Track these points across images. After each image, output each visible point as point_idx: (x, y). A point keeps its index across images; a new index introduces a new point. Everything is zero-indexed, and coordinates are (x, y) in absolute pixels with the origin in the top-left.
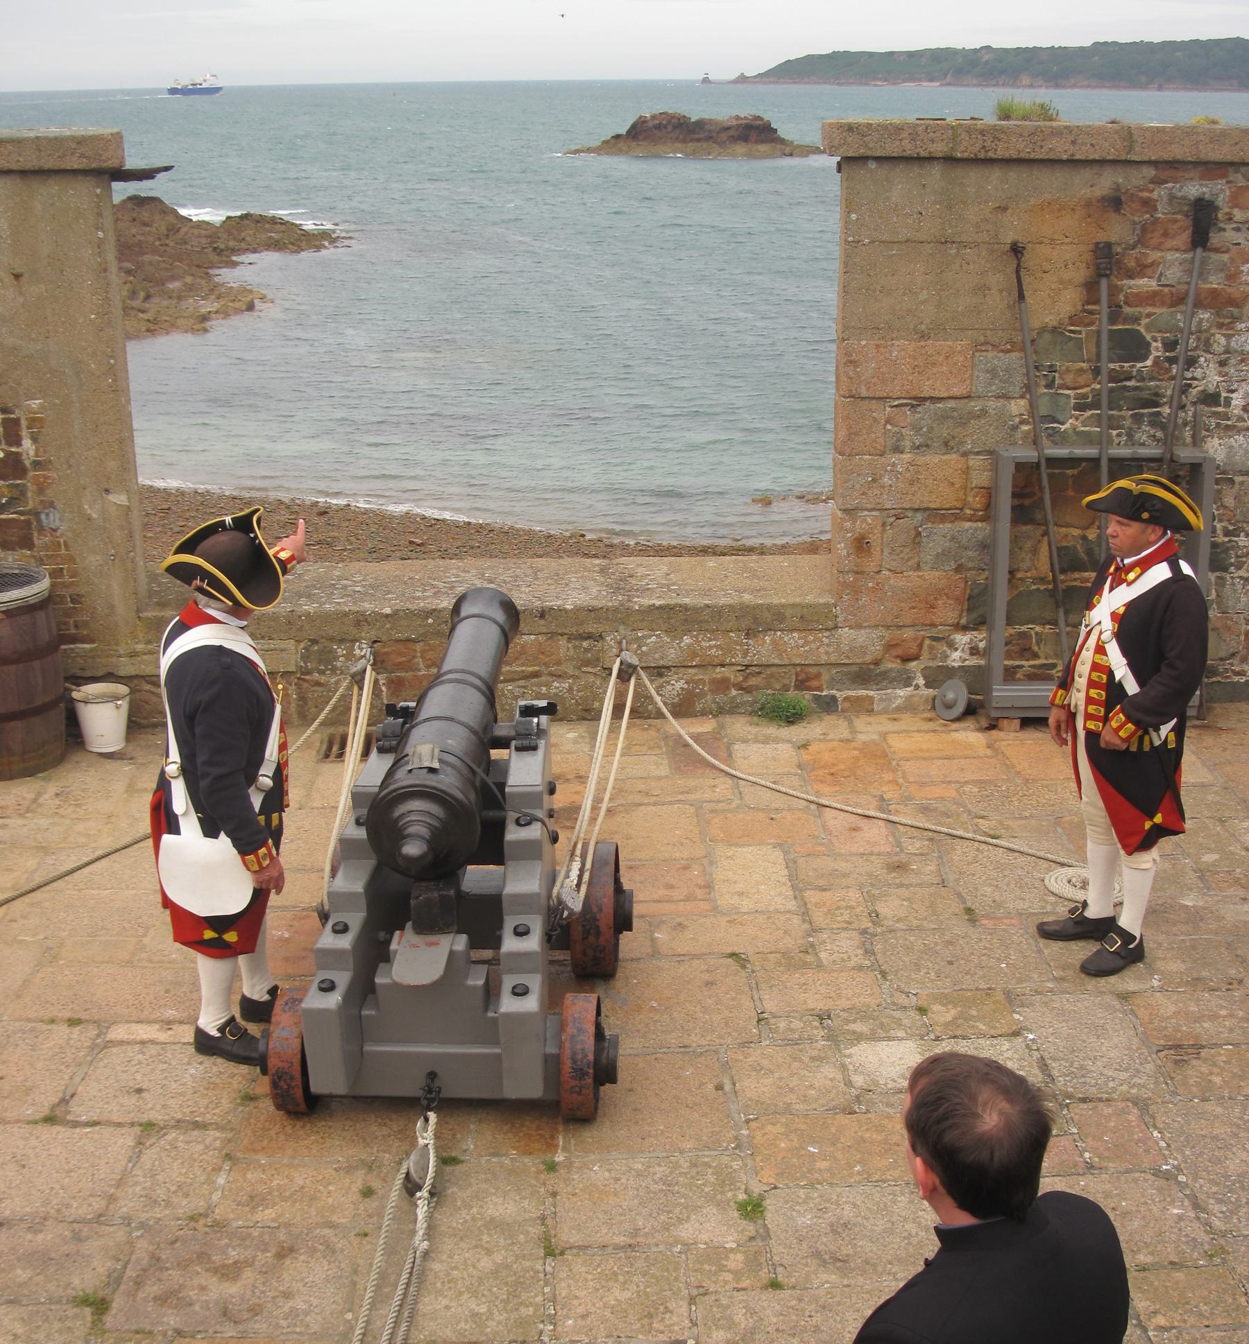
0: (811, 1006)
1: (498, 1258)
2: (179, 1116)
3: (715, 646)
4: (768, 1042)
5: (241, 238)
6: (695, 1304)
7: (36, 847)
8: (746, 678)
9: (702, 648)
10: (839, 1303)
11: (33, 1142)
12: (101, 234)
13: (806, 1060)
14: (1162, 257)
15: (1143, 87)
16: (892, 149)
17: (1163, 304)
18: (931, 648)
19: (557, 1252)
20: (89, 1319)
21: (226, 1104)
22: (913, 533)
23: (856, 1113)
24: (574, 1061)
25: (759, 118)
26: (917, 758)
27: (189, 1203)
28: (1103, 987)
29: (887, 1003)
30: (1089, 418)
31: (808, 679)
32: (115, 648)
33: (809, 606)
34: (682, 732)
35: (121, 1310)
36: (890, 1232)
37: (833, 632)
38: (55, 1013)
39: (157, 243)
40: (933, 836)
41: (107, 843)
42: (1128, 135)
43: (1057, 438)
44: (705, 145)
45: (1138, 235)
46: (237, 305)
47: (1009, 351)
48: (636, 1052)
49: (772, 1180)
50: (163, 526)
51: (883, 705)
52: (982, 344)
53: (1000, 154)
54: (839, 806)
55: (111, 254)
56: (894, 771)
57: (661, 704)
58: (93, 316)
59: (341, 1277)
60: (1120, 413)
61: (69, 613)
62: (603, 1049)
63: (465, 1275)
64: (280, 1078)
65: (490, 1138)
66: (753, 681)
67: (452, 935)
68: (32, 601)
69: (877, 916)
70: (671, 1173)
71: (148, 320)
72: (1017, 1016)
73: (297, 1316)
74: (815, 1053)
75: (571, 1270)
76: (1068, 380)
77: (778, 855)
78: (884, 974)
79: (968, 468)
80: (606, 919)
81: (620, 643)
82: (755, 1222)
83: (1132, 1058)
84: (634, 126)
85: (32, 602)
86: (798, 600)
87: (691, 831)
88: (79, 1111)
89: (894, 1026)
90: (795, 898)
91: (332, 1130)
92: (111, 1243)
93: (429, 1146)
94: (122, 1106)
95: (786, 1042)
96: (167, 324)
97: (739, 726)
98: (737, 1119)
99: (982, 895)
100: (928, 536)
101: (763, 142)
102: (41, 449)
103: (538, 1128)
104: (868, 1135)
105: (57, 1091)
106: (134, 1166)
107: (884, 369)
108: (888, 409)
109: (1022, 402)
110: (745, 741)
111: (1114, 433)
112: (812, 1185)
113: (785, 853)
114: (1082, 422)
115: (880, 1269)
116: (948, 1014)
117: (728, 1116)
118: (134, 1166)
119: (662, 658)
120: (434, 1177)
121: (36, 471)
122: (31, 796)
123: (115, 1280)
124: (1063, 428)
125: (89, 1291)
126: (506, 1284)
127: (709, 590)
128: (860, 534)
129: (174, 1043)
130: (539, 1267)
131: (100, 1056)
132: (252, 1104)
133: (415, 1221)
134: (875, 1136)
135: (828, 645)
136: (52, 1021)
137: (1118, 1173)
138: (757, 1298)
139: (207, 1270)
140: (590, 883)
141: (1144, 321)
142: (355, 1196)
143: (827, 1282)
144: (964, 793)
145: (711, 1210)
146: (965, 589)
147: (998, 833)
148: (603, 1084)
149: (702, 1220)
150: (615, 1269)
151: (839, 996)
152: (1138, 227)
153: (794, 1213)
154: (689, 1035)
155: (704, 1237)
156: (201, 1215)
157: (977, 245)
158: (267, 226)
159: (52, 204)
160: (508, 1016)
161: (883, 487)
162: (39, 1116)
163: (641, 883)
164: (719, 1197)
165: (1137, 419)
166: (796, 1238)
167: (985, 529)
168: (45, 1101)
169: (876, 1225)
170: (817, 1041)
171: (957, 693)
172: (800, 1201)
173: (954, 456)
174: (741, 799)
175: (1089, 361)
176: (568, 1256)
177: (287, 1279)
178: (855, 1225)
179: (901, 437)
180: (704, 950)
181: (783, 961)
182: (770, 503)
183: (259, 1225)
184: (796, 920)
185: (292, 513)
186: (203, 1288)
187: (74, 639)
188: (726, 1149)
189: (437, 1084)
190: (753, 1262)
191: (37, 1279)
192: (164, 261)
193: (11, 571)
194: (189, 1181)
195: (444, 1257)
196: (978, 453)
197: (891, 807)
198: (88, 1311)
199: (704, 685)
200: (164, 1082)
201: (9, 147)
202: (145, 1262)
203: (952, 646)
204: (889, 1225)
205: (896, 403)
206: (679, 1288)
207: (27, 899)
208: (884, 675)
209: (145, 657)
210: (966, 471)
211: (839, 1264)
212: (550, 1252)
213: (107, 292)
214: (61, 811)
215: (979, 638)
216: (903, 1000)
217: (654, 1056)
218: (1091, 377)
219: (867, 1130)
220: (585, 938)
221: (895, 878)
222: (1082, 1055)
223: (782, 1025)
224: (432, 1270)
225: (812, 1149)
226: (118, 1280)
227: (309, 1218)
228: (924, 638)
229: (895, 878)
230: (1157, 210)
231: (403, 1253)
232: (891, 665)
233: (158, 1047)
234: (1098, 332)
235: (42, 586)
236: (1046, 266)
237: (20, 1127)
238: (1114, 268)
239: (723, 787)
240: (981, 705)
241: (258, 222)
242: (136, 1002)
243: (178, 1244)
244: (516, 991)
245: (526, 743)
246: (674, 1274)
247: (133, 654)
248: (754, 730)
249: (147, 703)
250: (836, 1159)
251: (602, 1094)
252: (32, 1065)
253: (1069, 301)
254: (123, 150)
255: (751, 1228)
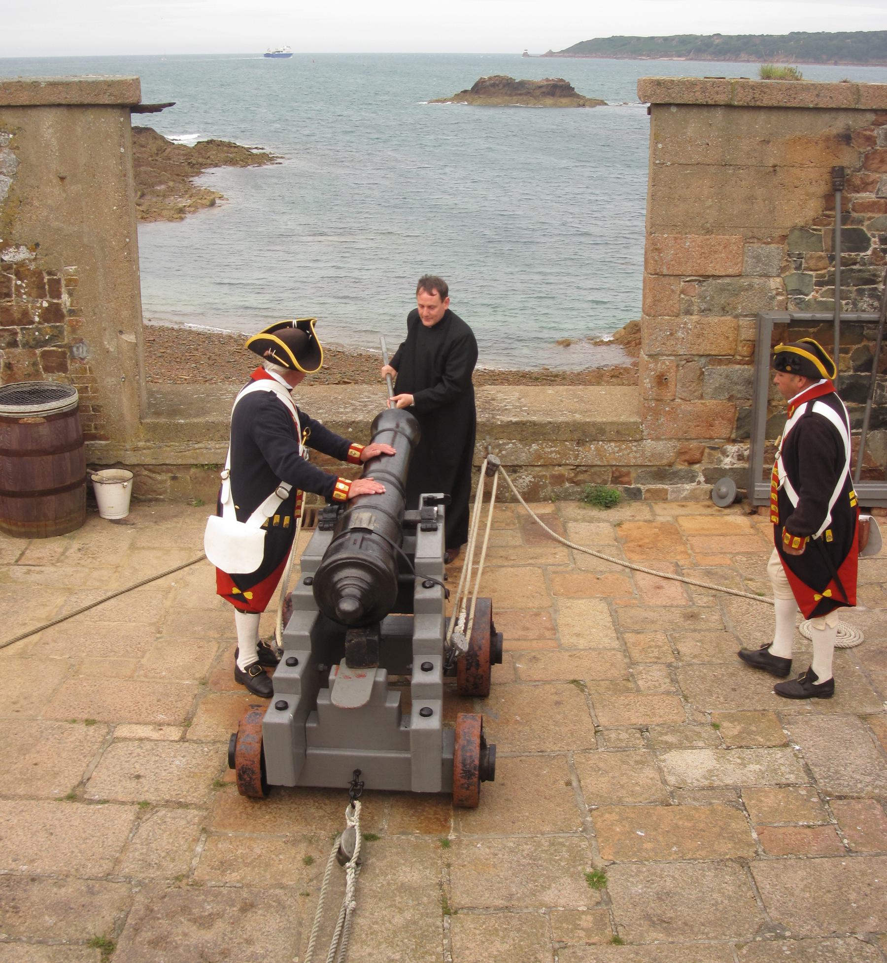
0: (634, 721)
1: (408, 915)
2: (167, 797)
3: (555, 451)
4: (603, 749)
5: (207, 156)
6: (558, 955)
7: (64, 589)
8: (576, 475)
9: (545, 453)
10: (666, 957)
11: (59, 815)
12: (122, 150)
13: (632, 763)
14: (878, 178)
15: (824, 62)
16: (688, 98)
17: (880, 211)
18: (710, 455)
19: (452, 911)
20: (99, 957)
21: (203, 789)
22: (698, 372)
23: (671, 805)
24: (464, 765)
25: (562, 80)
26: (701, 535)
27: (175, 866)
28: (848, 709)
29: (689, 720)
30: (826, 291)
31: (621, 476)
32: (123, 444)
33: (623, 424)
34: (532, 513)
35: (123, 951)
36: (702, 900)
37: (640, 443)
38: (76, 715)
39: (150, 159)
40: (716, 594)
41: (115, 586)
42: (856, 90)
43: (803, 306)
44: (525, 98)
45: (862, 161)
46: (204, 202)
47: (769, 243)
48: (506, 755)
49: (611, 857)
50: (150, 352)
51: (674, 495)
52: (750, 238)
53: (766, 102)
54: (646, 570)
55: (129, 165)
56: (685, 544)
57: (517, 493)
58: (115, 208)
59: (290, 928)
60: (848, 288)
61: (90, 419)
62: (485, 755)
63: (384, 929)
64: (244, 772)
65: (399, 820)
66: (581, 477)
67: (375, 669)
68: (65, 410)
69: (678, 653)
70: (536, 850)
71: (143, 211)
72: (785, 732)
73: (257, 959)
74: (638, 758)
75: (463, 926)
76: (811, 265)
77: (603, 606)
78: (686, 698)
79: (738, 326)
80: (484, 654)
81: (486, 448)
82: (600, 890)
83: (873, 765)
84: (476, 85)
85: (64, 411)
86: (615, 419)
87: (540, 587)
88: (94, 791)
89: (695, 738)
90: (618, 638)
91: (282, 811)
92: (116, 897)
93: (356, 827)
94: (125, 788)
95: (616, 749)
96: (155, 214)
97: (571, 509)
98: (582, 808)
99: (754, 638)
100: (709, 375)
101: (564, 96)
102: (75, 302)
103: (435, 813)
104: (681, 823)
105: (77, 776)
106: (134, 836)
107: (680, 255)
108: (682, 284)
109: (778, 280)
110: (576, 520)
111: (844, 302)
112: (641, 862)
113: (609, 604)
114: (821, 294)
115: (696, 929)
116: (736, 729)
117: (576, 806)
118: (134, 836)
119: (516, 459)
120: (359, 852)
121: (70, 316)
122: (60, 550)
123: (119, 926)
124: (807, 298)
125: (100, 935)
126: (414, 936)
127: (551, 410)
128: (660, 372)
129: (164, 741)
130: (439, 923)
131: (109, 749)
132: (222, 789)
133: (346, 884)
134: (686, 824)
135: (636, 452)
136: (74, 721)
137: (870, 855)
138: (604, 952)
139: (189, 920)
140: (473, 629)
141: (866, 223)
142: (300, 864)
143: (656, 939)
144: (736, 561)
145: (566, 880)
146: (735, 413)
147: (762, 592)
148: (483, 781)
149: (560, 888)
150: (496, 926)
151: (654, 714)
152: (863, 156)
153: (629, 884)
154: (545, 742)
155: (562, 901)
156: (184, 876)
157: (748, 167)
158: (225, 148)
159: (89, 129)
160: (417, 732)
161: (677, 339)
162: (63, 795)
163: (505, 625)
164: (572, 869)
165: (860, 292)
166: (632, 904)
167: (750, 371)
168: (67, 783)
169: (691, 894)
170: (639, 749)
171: (729, 488)
172: (633, 874)
173: (729, 318)
174: (575, 563)
175: (827, 250)
176: (460, 915)
177: (249, 929)
178: (674, 894)
179: (691, 304)
180: (552, 677)
181: (611, 686)
182: (568, 345)
183: (227, 885)
184: (619, 656)
185: (238, 345)
186: (185, 935)
187: (94, 437)
188: (576, 832)
189: (360, 780)
190: (600, 923)
191: (59, 924)
192: (154, 171)
193: (50, 388)
194: (175, 848)
195: (367, 914)
196: (746, 316)
197: (684, 571)
198: (98, 951)
199: (546, 479)
200: (157, 771)
201: (60, 88)
202: (142, 912)
203: (725, 453)
204: (701, 894)
205: (687, 279)
206: (545, 942)
207: (57, 627)
208: (675, 474)
209: (144, 451)
210: (738, 328)
211: (665, 925)
212: (447, 911)
213: (126, 191)
214: (82, 562)
215: (745, 448)
216: (700, 718)
217: (519, 759)
218: (828, 262)
219: (680, 818)
220: (468, 669)
221: (689, 624)
222: (836, 763)
223: (613, 736)
224: (358, 924)
225: (639, 833)
226: (121, 928)
227: (265, 880)
228: (704, 448)
229: (689, 624)
230: (876, 144)
231: (336, 910)
232: (681, 467)
233: (152, 744)
234: (834, 231)
235: (73, 399)
236: (797, 183)
237: (49, 803)
238: (846, 185)
239: (561, 554)
240: (745, 496)
241: (219, 145)
242: (136, 708)
243: (166, 899)
244: (423, 713)
245: (429, 526)
246: (541, 931)
247: (136, 449)
248: (582, 512)
249: (145, 484)
250: (658, 841)
251: (481, 787)
252: (59, 755)
253: (813, 208)
254: (140, 91)
255: (597, 895)
